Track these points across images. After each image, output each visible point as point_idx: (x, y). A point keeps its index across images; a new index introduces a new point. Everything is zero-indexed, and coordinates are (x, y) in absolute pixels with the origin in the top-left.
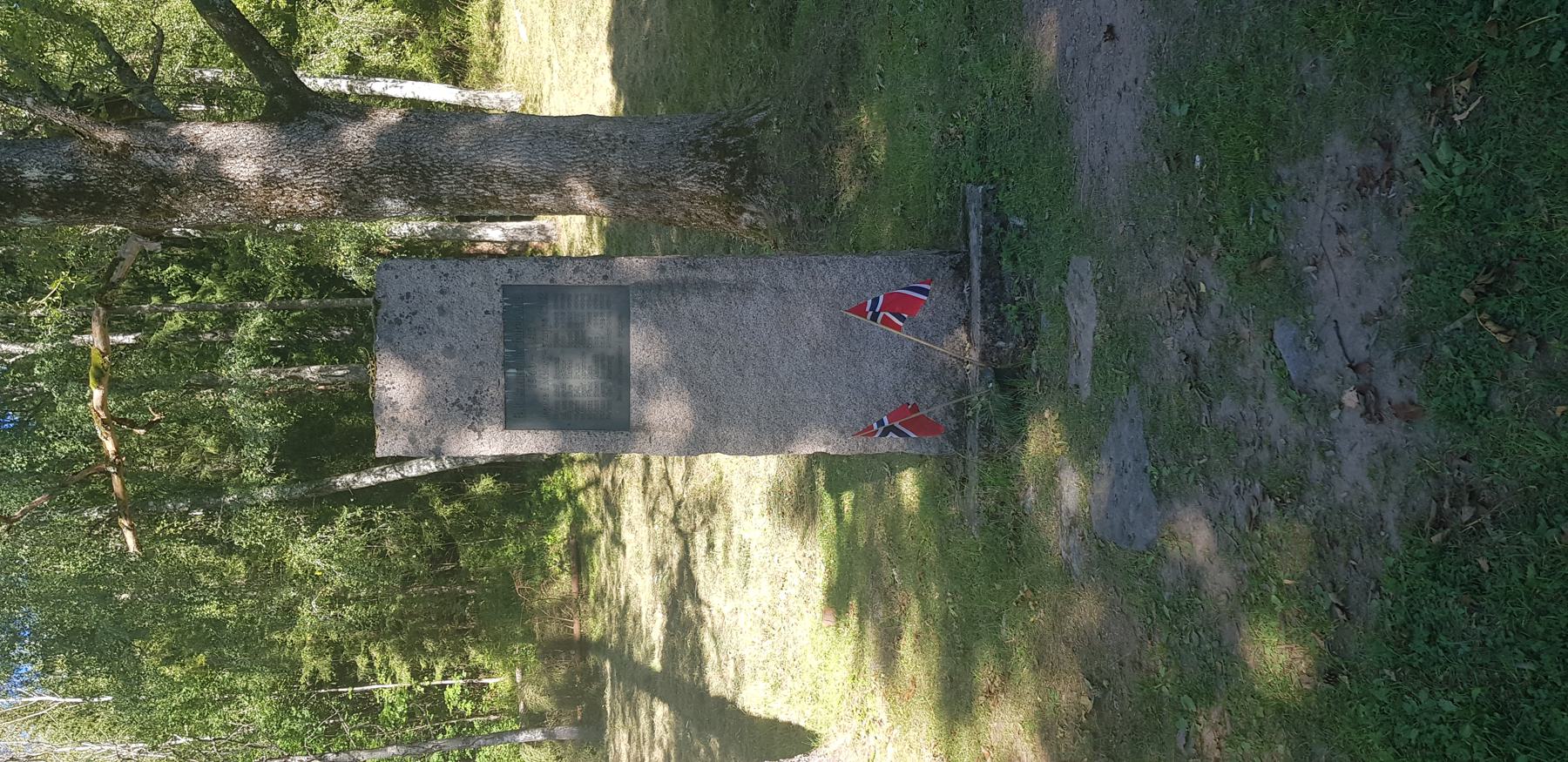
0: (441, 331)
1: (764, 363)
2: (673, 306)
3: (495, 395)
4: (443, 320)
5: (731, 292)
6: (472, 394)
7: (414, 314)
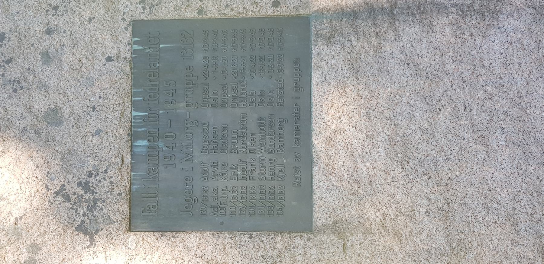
0: (44, 86)
1: (519, 125)
2: (374, 41)
3: (116, 178)
4: (48, 69)
5: (464, 17)
6: (84, 178)
7: (9, 61)
